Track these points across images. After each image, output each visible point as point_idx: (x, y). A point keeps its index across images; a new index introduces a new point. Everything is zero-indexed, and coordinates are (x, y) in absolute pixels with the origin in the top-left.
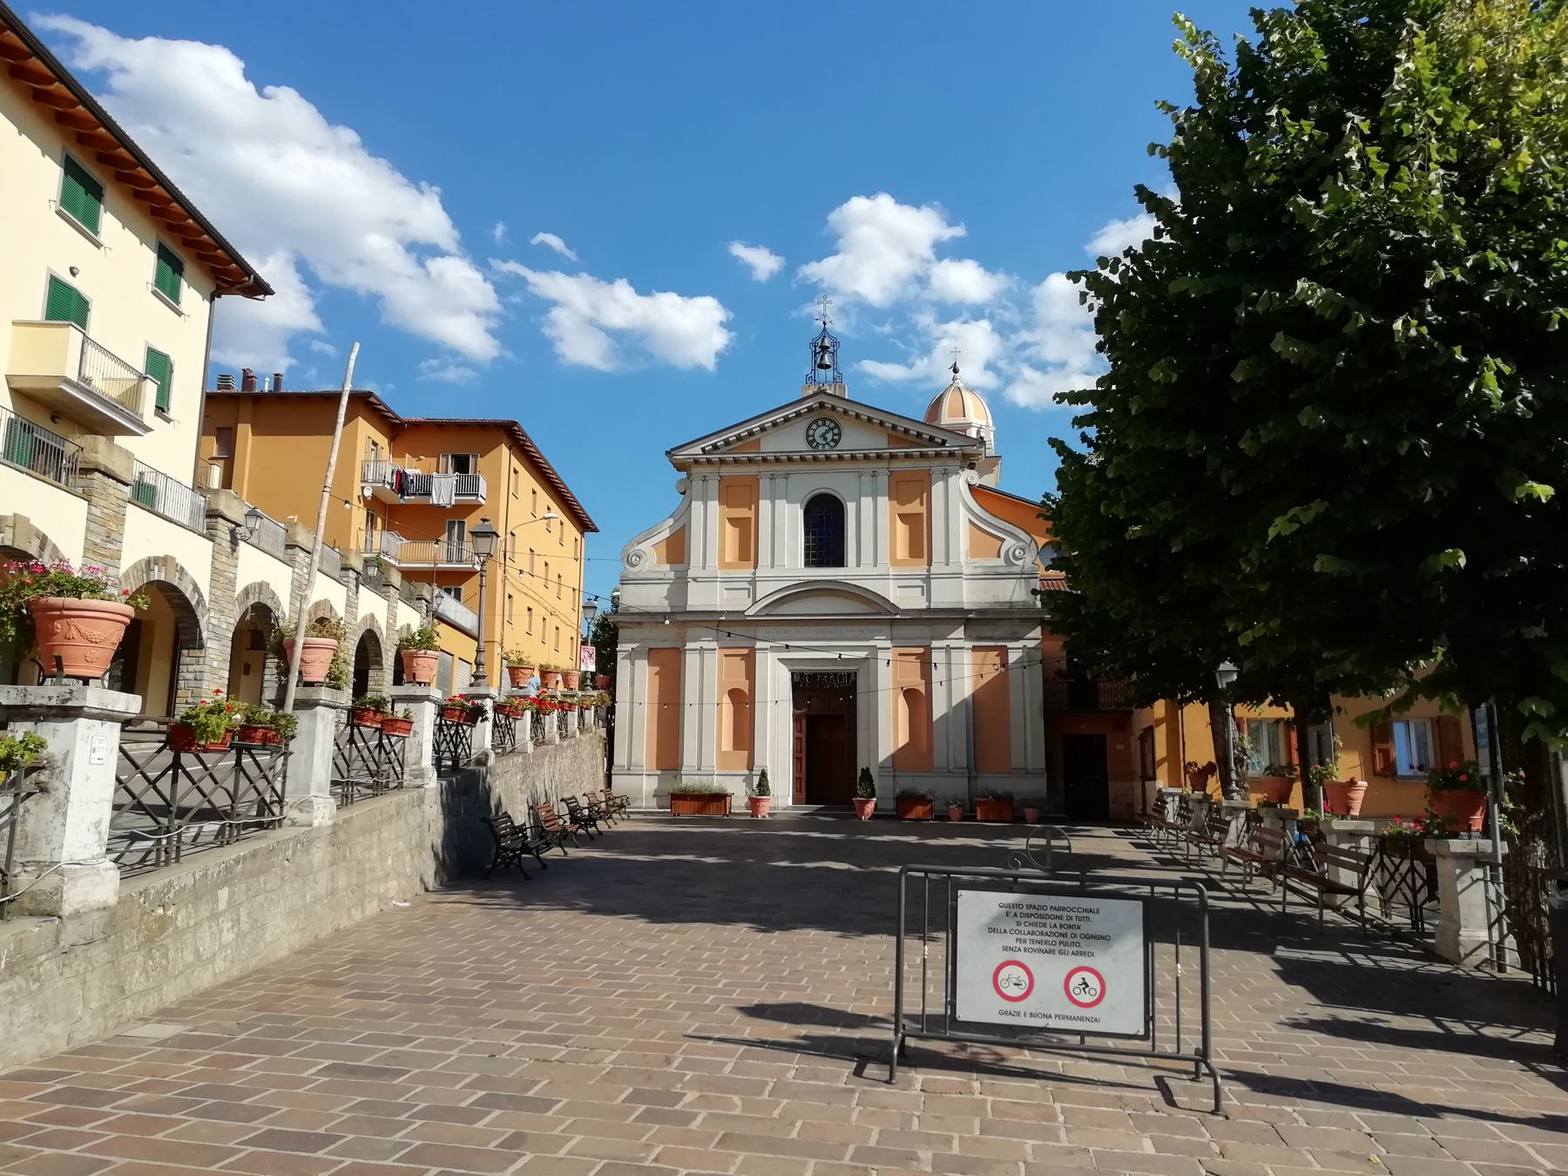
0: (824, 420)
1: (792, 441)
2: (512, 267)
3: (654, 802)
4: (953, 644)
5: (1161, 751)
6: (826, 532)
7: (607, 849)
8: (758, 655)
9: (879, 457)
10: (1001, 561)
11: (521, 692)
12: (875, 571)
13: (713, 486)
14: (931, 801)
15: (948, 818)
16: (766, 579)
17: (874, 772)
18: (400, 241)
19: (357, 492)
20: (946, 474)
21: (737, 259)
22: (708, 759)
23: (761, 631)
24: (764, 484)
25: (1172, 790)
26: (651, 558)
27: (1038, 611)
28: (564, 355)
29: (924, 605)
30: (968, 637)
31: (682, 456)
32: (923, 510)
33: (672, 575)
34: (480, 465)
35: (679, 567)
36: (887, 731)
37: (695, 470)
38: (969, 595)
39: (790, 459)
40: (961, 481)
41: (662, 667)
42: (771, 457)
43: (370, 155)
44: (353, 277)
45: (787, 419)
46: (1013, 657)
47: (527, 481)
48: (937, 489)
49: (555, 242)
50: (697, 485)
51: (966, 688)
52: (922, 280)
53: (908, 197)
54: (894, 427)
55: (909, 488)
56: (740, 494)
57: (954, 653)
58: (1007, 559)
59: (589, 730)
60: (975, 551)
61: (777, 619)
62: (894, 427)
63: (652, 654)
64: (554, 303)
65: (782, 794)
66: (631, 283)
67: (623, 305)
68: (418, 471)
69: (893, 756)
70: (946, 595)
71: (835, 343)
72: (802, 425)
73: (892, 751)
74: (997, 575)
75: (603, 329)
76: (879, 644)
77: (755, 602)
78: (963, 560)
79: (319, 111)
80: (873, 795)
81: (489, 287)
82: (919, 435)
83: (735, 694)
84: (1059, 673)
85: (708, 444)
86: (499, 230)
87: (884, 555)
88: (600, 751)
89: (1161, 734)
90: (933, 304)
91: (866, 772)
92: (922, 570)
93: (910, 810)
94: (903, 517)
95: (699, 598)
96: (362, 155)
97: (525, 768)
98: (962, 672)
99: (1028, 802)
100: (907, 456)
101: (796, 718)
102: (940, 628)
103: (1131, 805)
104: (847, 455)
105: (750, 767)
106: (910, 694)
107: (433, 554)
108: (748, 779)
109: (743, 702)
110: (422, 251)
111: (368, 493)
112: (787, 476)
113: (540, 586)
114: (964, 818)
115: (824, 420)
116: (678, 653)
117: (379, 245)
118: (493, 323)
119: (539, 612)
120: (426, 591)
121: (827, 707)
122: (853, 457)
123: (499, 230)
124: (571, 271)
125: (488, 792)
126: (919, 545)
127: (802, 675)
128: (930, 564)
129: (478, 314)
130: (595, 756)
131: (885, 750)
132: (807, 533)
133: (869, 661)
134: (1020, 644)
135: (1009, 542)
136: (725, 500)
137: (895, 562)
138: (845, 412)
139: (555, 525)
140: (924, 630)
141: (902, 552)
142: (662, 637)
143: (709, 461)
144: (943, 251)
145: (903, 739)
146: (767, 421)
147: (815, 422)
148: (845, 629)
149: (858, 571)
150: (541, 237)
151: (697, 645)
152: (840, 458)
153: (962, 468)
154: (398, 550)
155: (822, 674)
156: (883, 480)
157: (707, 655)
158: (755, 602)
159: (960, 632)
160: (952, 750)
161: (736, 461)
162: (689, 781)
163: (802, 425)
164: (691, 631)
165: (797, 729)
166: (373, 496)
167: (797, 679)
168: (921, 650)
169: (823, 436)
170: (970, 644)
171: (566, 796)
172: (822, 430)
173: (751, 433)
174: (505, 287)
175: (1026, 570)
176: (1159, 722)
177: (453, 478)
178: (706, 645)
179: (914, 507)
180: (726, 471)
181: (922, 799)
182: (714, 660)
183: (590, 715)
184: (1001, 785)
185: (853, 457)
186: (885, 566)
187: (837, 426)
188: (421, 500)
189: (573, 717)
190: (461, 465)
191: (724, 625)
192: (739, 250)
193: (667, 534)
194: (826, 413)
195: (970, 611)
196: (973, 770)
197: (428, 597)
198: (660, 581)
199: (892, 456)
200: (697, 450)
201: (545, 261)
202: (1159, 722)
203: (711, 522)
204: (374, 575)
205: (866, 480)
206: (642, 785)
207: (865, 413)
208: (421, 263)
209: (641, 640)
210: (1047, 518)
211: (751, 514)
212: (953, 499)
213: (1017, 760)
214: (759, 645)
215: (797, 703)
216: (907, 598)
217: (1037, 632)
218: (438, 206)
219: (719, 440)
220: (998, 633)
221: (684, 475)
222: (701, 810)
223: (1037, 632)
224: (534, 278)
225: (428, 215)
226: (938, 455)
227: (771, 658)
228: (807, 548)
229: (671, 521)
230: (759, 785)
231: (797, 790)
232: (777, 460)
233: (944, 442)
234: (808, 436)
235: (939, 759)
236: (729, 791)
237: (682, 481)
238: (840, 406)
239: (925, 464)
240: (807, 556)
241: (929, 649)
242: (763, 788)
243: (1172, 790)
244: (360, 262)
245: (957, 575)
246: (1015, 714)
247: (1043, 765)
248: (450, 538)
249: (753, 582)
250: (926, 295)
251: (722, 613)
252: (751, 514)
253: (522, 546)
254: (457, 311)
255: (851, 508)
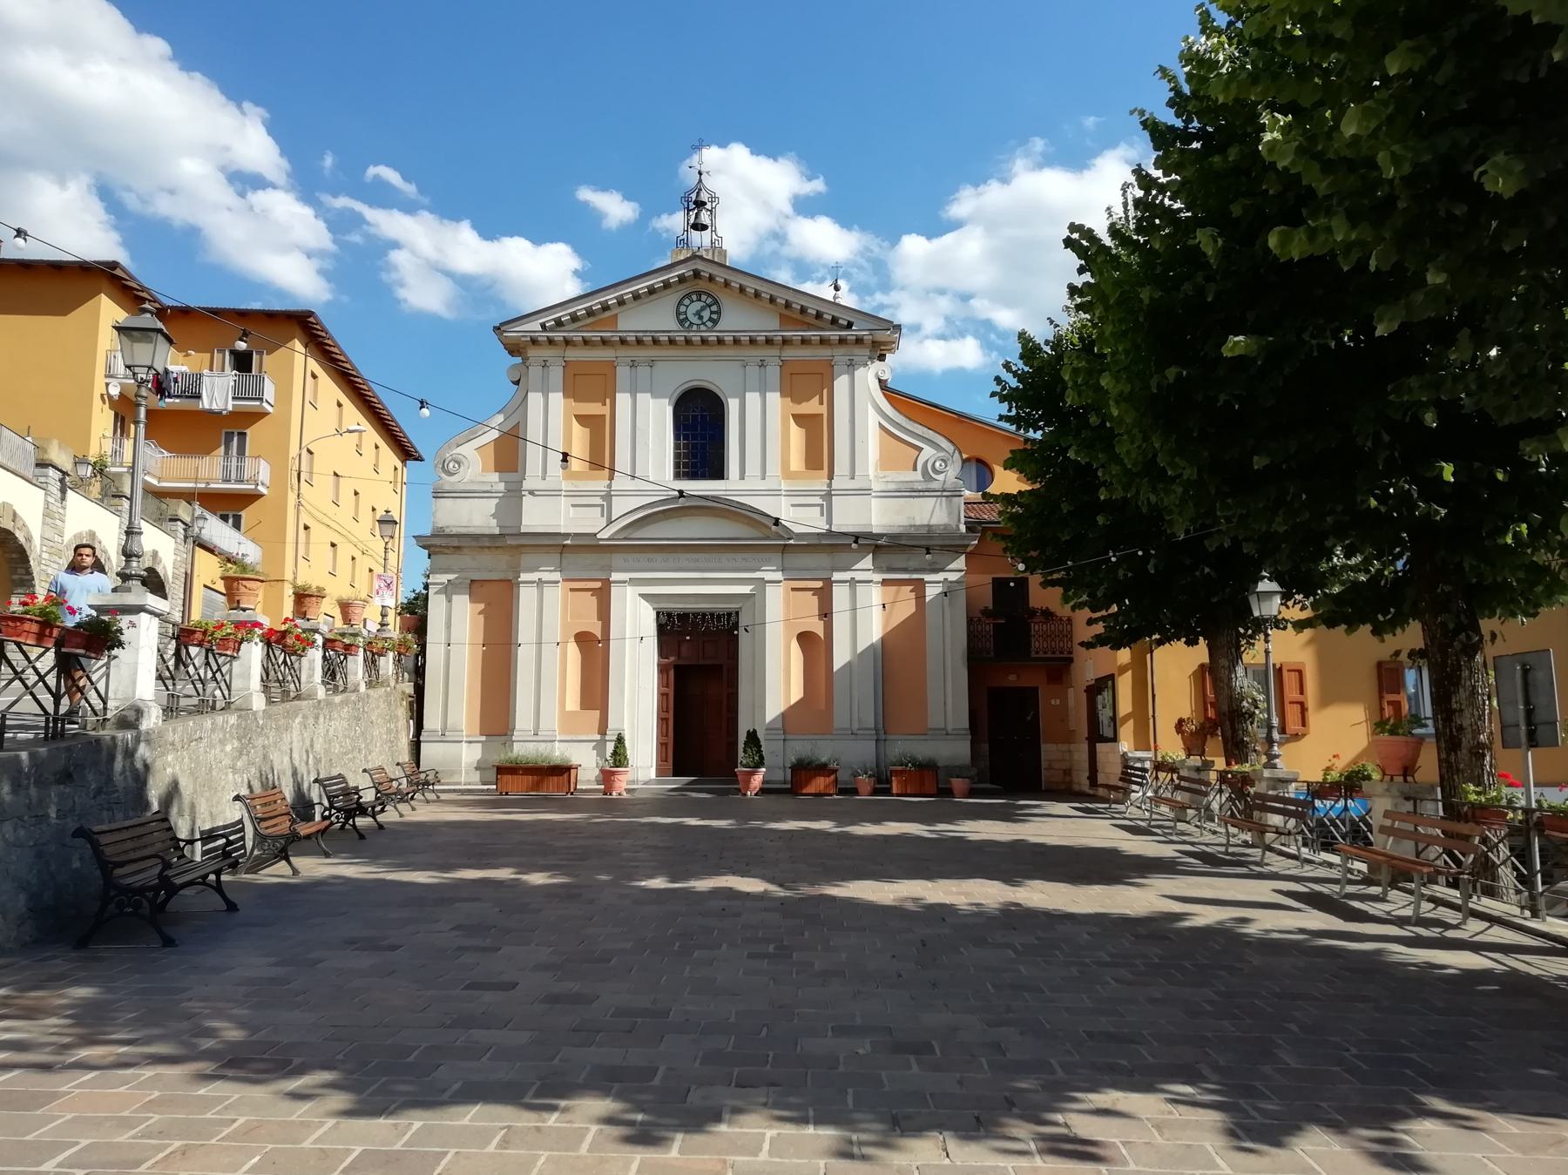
0: (699, 294)
1: (659, 318)
2: (342, 202)
3: (476, 776)
4: (859, 576)
5: (1125, 705)
6: (701, 435)
7: (374, 857)
8: (614, 590)
9: (769, 342)
10: (918, 475)
11: (242, 616)
12: (762, 485)
13: (556, 373)
14: (835, 771)
15: (855, 792)
16: (625, 494)
17: (760, 735)
18: (223, 169)
19: (99, 388)
20: (851, 366)
21: (586, 204)
22: (547, 722)
23: (617, 559)
24: (623, 372)
25: (1139, 754)
26: (473, 461)
27: (962, 537)
28: (405, 301)
29: (820, 525)
30: (877, 568)
31: (514, 333)
32: (823, 410)
33: (501, 487)
34: (268, 363)
35: (512, 476)
36: (776, 684)
37: (532, 352)
38: (879, 517)
39: (656, 342)
40: (869, 375)
41: (488, 604)
42: (631, 338)
43: (182, 68)
44: (164, 207)
45: (652, 291)
46: (931, 592)
47: (330, 390)
48: (841, 384)
49: (391, 176)
50: (535, 371)
51: (874, 629)
52: (779, 236)
53: (765, 147)
54: (788, 305)
55: (807, 381)
56: (591, 385)
57: (860, 588)
58: (925, 473)
59: (385, 684)
60: (886, 463)
61: (637, 545)
62: (788, 305)
63: (475, 588)
64: (395, 245)
65: (644, 764)
66: (475, 227)
67: (467, 249)
68: (184, 369)
69: (783, 715)
70: (850, 516)
71: (713, 198)
72: (672, 299)
73: (782, 709)
74: (913, 492)
75: (448, 274)
76: (768, 576)
77: (610, 522)
78: (871, 472)
79: (125, 15)
80: (760, 763)
81: (321, 225)
82: (819, 315)
83: (583, 639)
84: (985, 612)
85: (549, 319)
86: (328, 161)
87: (774, 467)
88: (402, 712)
89: (1125, 685)
90: (789, 260)
91: (752, 737)
92: (821, 484)
93: (808, 782)
94: (799, 419)
95: (537, 516)
96: (172, 69)
97: (245, 736)
98: (868, 611)
99: (955, 771)
100: (805, 342)
101: (662, 669)
102: (843, 557)
103: (1068, 772)
104: (728, 338)
105: (603, 729)
106: (805, 639)
107: (210, 471)
108: (600, 746)
109: (594, 650)
110: (245, 182)
111: (115, 391)
112: (651, 363)
113: (338, 508)
114: (875, 792)
115: (699, 294)
116: (509, 587)
117: (193, 169)
118: (328, 264)
119: (345, 551)
120: (183, 510)
121: (702, 658)
122: (736, 342)
123: (328, 161)
124: (409, 208)
125: (140, 778)
126: (818, 455)
127: (669, 615)
128: (831, 477)
129: (309, 255)
130: (393, 718)
131: (774, 707)
132: (677, 437)
133: (755, 600)
134: (940, 576)
135: (928, 452)
136: (571, 392)
137: (788, 474)
138: (727, 284)
139: (368, 449)
140: (822, 559)
141: (797, 462)
142: (490, 566)
143: (551, 341)
144: (805, 207)
145: (797, 694)
146: (627, 291)
147: (688, 296)
148: (725, 558)
149: (743, 485)
150: (372, 171)
151: (534, 576)
152: (720, 342)
153: (871, 358)
154: (161, 466)
155: (696, 615)
156: (773, 372)
157: (547, 590)
158: (610, 522)
159: (867, 562)
160: (857, 707)
161: (586, 342)
162: (524, 749)
163: (672, 299)
164: (527, 559)
165: (663, 683)
166: (121, 395)
167: (664, 620)
168: (819, 584)
169: (698, 314)
170: (878, 577)
171: (370, 766)
172: (697, 306)
173: (605, 308)
174: (340, 224)
175: (947, 486)
176: (1123, 670)
177: (230, 376)
178: (546, 576)
179: (812, 407)
180: (572, 354)
181: (823, 769)
182: (556, 596)
183: (387, 664)
184: (923, 750)
185: (736, 342)
186: (775, 479)
187: (716, 302)
188: (188, 404)
189: (356, 666)
190: (242, 363)
191: (564, 549)
192: (586, 194)
193: (495, 434)
194: (702, 285)
195: (881, 536)
196: (882, 732)
197: (188, 519)
198: (485, 494)
199: (786, 342)
200: (535, 326)
201: (383, 197)
202: (1123, 670)
203: (552, 417)
204: (106, 486)
205: (753, 370)
206: (459, 755)
207: (751, 286)
208: (242, 195)
209: (461, 570)
210: (1003, 399)
211: (606, 410)
212: (859, 394)
213: (935, 720)
214: (615, 576)
215: (663, 650)
216: (802, 519)
217: (960, 562)
218: (262, 130)
219: (564, 314)
220: (912, 564)
221: (518, 360)
222: (536, 786)
223: (960, 562)
224: (371, 214)
225: (255, 145)
226: (842, 341)
227: (631, 592)
228: (677, 456)
229: (500, 418)
230: (615, 753)
231: (662, 758)
232: (639, 342)
233: (850, 325)
234: (678, 313)
235: (841, 719)
236: (574, 762)
237: (514, 366)
238: (721, 275)
239: (824, 352)
240: (677, 465)
241: (829, 583)
242: (619, 757)
243: (1139, 754)
244: (172, 192)
245: (865, 492)
246: (932, 664)
247: (966, 725)
248: (226, 453)
249: (608, 497)
250: (785, 251)
251: (567, 535)
252: (606, 410)
253: (324, 464)
254: (286, 248)
255: (733, 406)
